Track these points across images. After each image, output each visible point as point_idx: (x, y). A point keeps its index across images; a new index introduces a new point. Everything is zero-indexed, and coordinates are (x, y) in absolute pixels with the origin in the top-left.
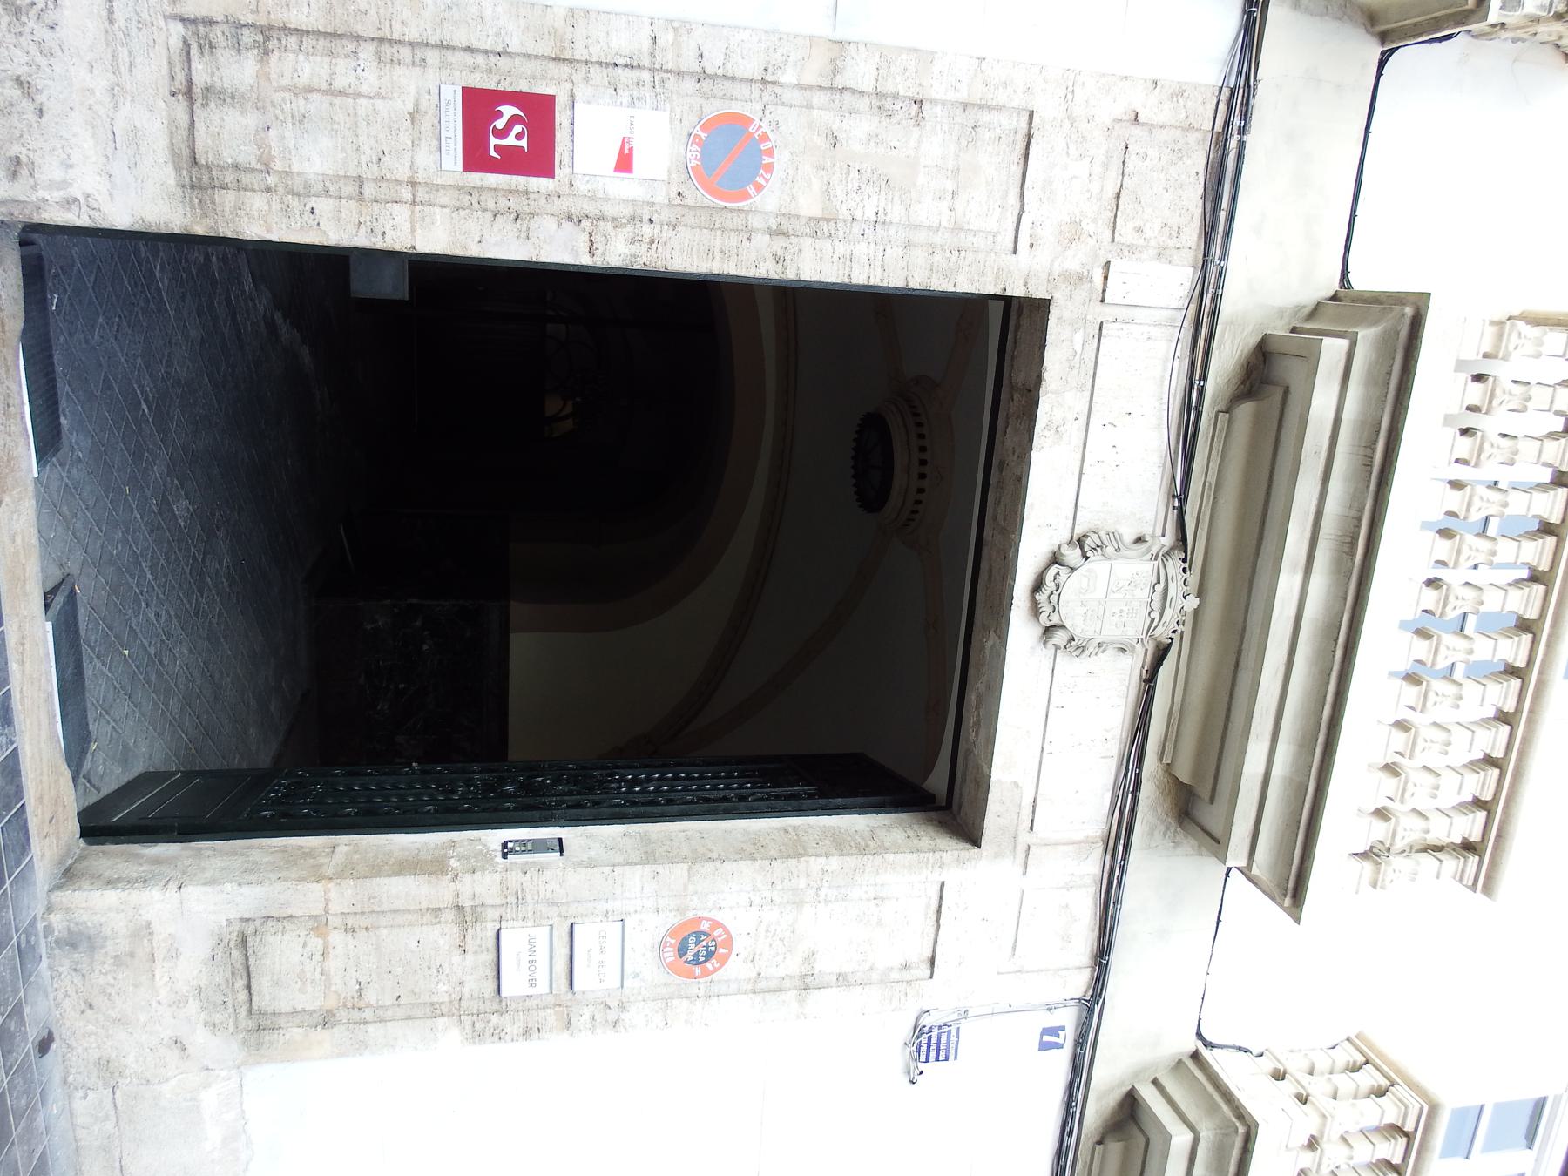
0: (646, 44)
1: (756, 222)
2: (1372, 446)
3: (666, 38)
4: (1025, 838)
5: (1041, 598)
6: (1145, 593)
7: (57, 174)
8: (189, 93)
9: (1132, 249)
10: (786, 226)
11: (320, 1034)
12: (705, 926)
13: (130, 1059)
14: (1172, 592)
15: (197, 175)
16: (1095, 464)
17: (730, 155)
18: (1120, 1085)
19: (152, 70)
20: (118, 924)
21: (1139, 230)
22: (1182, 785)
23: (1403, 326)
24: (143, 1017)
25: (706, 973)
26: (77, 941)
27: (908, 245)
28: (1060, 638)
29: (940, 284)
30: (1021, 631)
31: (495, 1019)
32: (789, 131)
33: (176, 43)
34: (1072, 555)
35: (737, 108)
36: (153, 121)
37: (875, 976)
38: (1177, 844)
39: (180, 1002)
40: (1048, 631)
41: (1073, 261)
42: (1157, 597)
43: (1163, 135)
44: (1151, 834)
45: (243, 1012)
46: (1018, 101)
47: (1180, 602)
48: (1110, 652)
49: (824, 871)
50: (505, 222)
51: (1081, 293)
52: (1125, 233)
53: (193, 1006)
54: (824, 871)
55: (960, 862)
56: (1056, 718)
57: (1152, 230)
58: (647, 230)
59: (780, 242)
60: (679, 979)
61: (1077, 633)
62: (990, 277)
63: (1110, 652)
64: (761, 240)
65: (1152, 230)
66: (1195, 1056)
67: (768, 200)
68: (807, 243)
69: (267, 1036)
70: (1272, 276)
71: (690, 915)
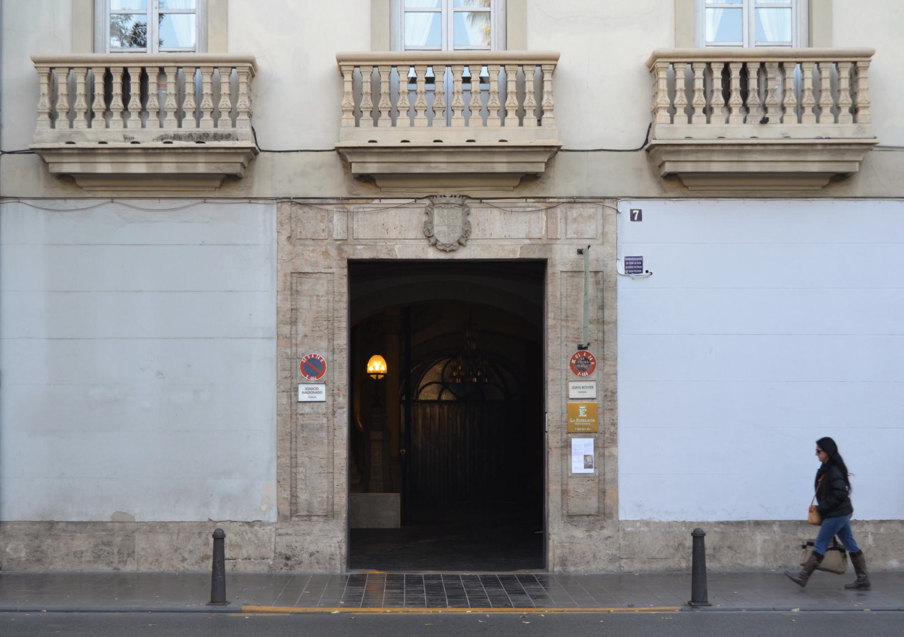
0: (285, 394)
1: (331, 358)
2: (385, 153)
3: (282, 388)
4: (544, 241)
5: (448, 250)
6: (445, 211)
7: (333, 549)
8: (309, 516)
9: (329, 231)
10: (331, 348)
11: (608, 492)
12: (574, 362)
13: (610, 553)
14: (444, 201)
15: (329, 515)
16: (399, 232)
17: (313, 368)
18: (659, 183)
19: (304, 526)
20: (558, 552)
21: (323, 230)
22: (525, 175)
23: (343, 153)
24: (593, 547)
25: (594, 360)
26: (563, 562)
27: (334, 310)
28: (463, 241)
29: (345, 298)
30: (463, 254)
31: (607, 435)
32: (305, 351)
33: (297, 519)
34: (433, 240)
35: (299, 366)
36: (318, 526)
37: (600, 295)
38: (549, 177)
39: (590, 536)
40: (460, 244)
41: (333, 252)
42: (447, 206)
43: (294, 227)
44: (543, 189)
45: (598, 518)
46: (289, 278)
47: (448, 198)
48: (470, 218)
49: (554, 319)
50: (337, 433)
51: (345, 248)
52: (324, 235)
53: (593, 533)
54: (554, 319)
55: (554, 266)
56: (498, 233)
57: (323, 226)
58: (336, 392)
59: (336, 350)
60: (596, 370)
61: (460, 235)
62: (341, 281)
63: (470, 218)
64: (336, 357)
65: (323, 226)
66: (648, 151)
67: (323, 355)
68: (335, 342)
69: (607, 511)
70: (332, 184)
71: (569, 367)
